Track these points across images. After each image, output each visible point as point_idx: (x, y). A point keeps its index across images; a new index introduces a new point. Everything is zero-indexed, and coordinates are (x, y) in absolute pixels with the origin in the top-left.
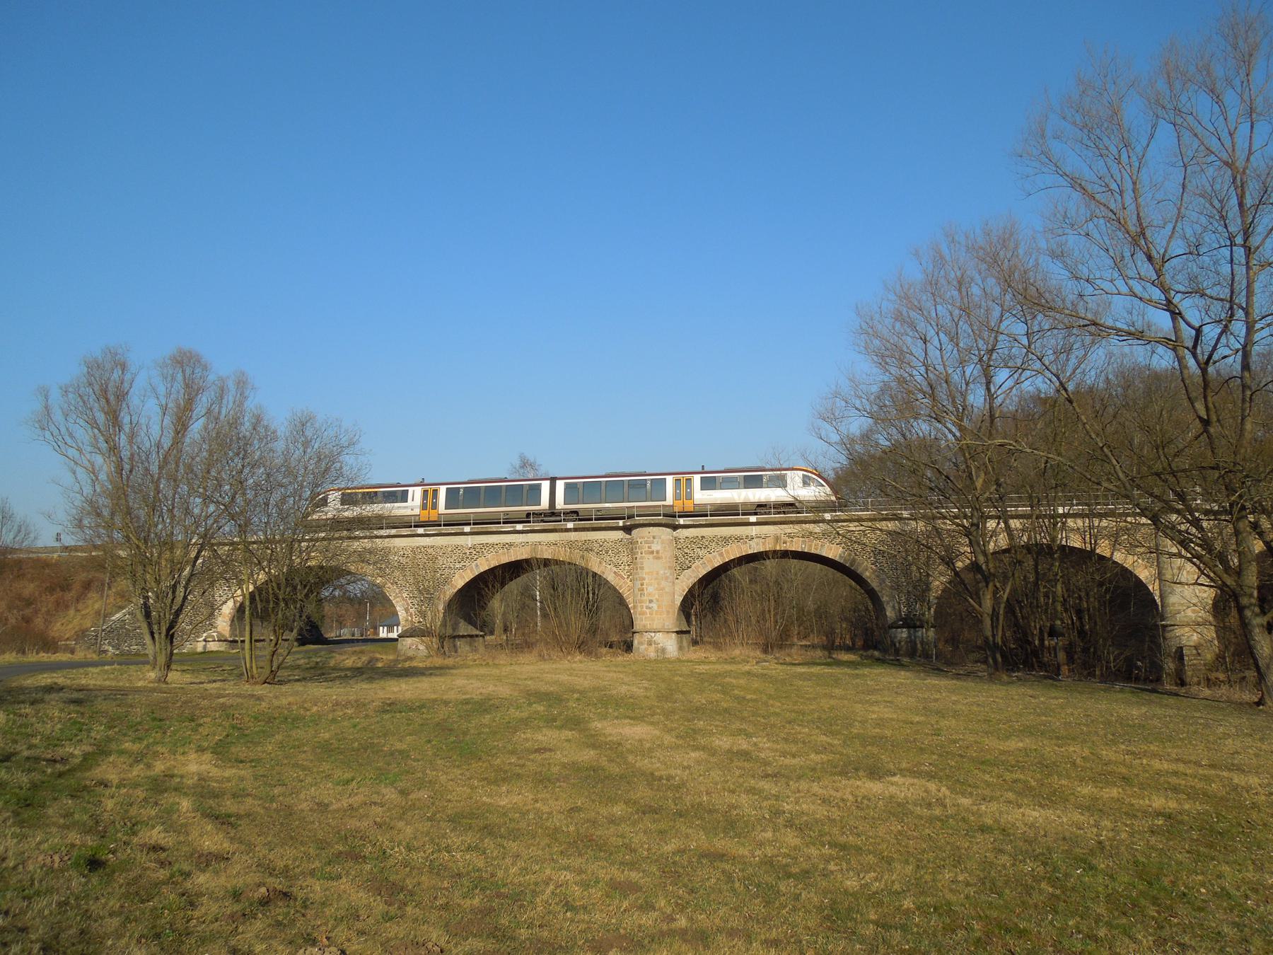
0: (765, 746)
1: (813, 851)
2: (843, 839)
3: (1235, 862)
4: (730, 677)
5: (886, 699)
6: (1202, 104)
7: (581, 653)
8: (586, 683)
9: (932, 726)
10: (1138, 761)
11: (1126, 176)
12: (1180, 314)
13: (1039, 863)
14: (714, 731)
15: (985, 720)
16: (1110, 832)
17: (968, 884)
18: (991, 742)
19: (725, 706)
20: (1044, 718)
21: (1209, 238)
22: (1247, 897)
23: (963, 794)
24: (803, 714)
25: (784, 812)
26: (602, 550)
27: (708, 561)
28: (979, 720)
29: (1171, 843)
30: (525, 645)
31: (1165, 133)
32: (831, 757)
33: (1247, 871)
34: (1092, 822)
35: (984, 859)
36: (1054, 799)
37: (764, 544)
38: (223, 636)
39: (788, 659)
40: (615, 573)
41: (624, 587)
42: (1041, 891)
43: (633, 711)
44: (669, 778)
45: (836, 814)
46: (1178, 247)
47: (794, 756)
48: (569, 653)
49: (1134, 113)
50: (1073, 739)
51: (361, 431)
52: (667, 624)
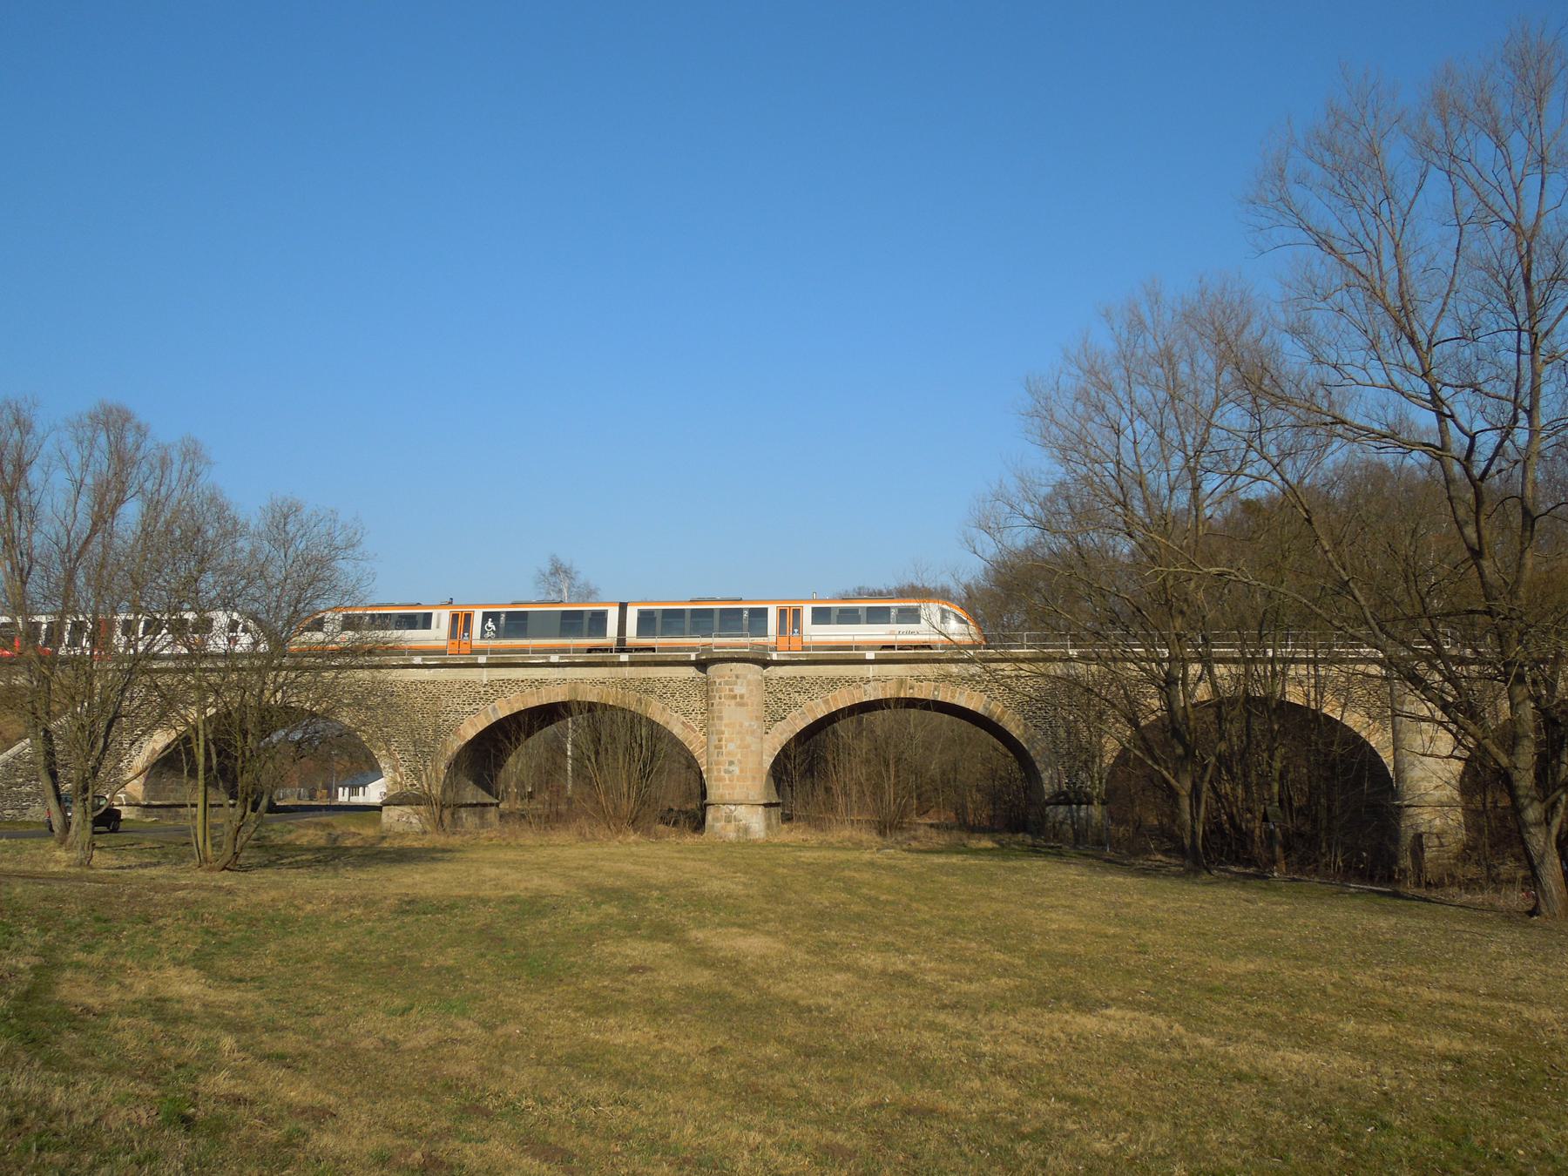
0: (931, 969)
1: (1040, 1106)
2: (1070, 1090)
3: (1549, 1117)
4: (850, 870)
5: (1064, 902)
6: (1484, 149)
8: (662, 875)
9: (1133, 941)
10: (1403, 989)
11: (1384, 234)
12: (1452, 416)
13: (1320, 1120)
15: (1199, 933)
16: (1394, 1081)
17: (1242, 1147)
18: (1213, 963)
20: (1272, 931)
21: (1486, 319)
24: (962, 922)
26: (667, 691)
27: (808, 711)
28: (1191, 934)
29: (1469, 1094)
30: (553, 819)
32: (1018, 982)
34: (1368, 1068)
35: (1252, 1116)
37: (883, 689)
38: (134, 798)
40: (683, 723)
41: (694, 742)
42: (1333, 1155)
44: (820, 1009)
46: (1447, 329)
47: (970, 980)
48: (619, 832)
49: (1398, 156)
52: (752, 793)
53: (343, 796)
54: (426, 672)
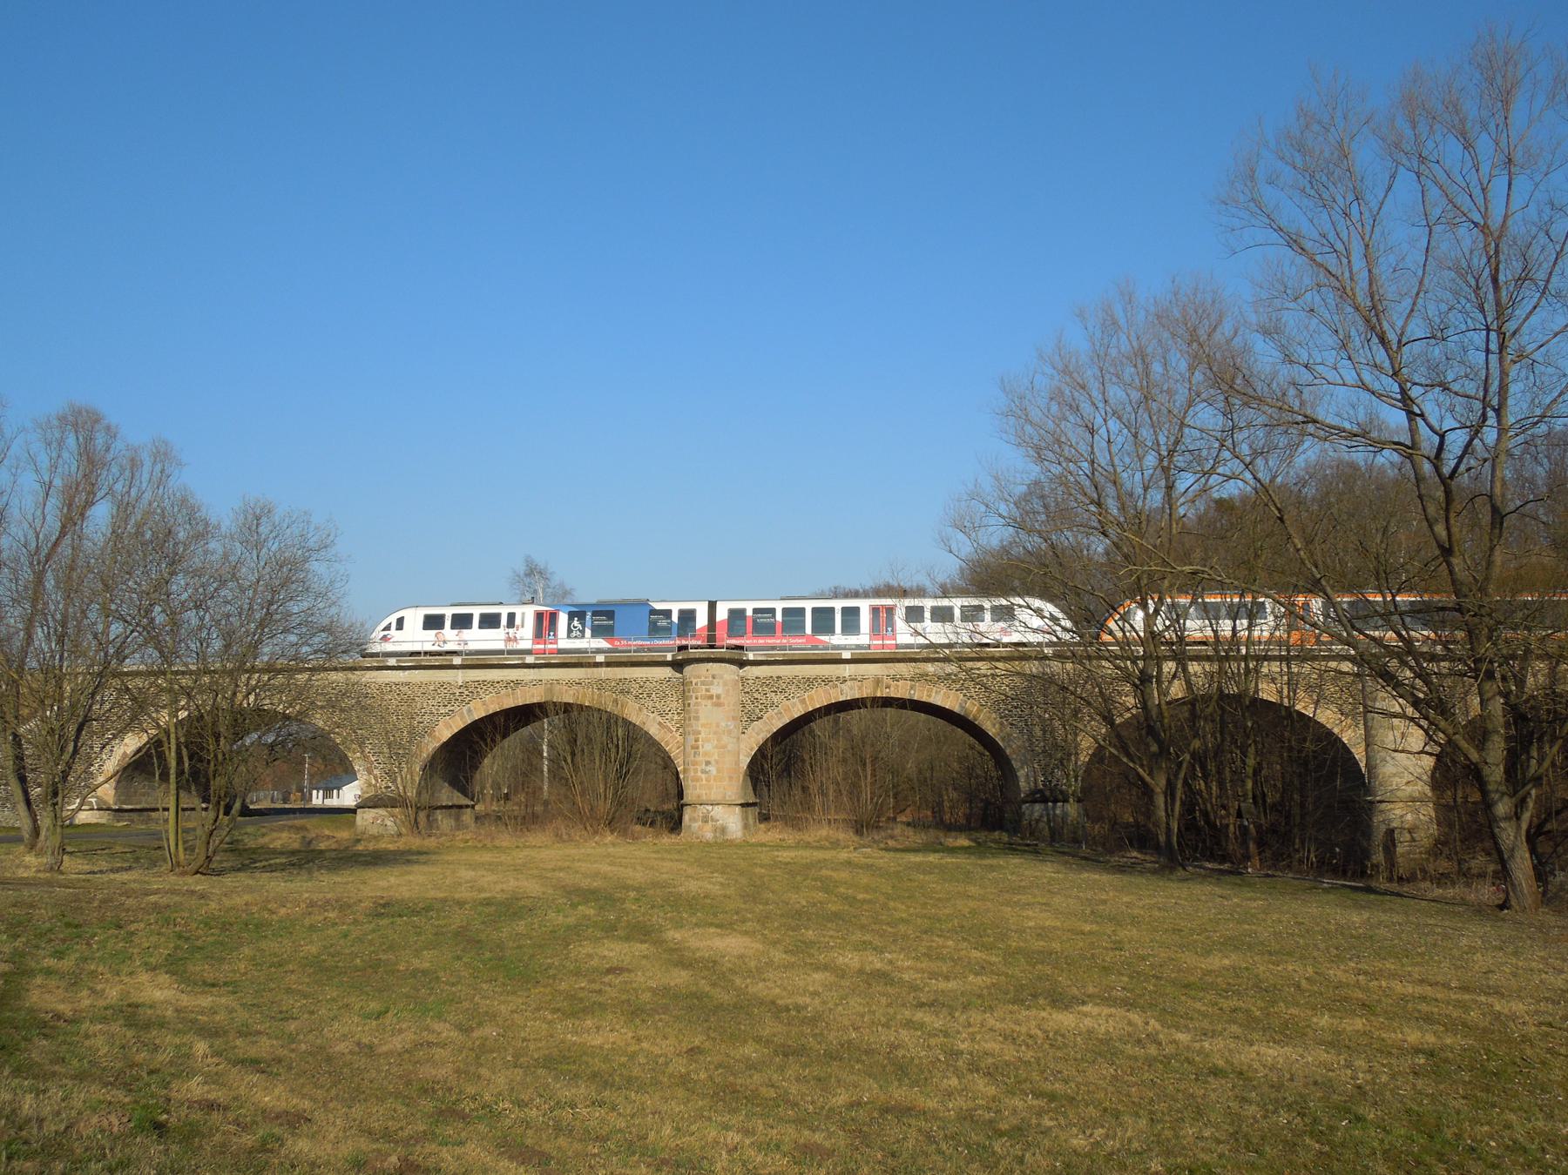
0: (907, 966)
1: (1017, 1102)
2: (1048, 1087)
4: (827, 869)
6: (1452, 151)
7: (612, 832)
9: (1109, 937)
10: (1376, 983)
12: (1422, 415)
14: (831, 944)
17: (1219, 1142)
18: (1189, 959)
19: (834, 909)
20: (1247, 927)
22: (1543, 1150)
23: (1177, 1028)
24: (939, 920)
25: (962, 1053)
26: (643, 693)
28: (1167, 930)
30: (529, 821)
31: (1406, 184)
33: (1537, 1119)
34: (1342, 1062)
36: (1288, 1032)
37: (860, 688)
38: (105, 803)
39: (891, 843)
40: (660, 723)
41: (671, 742)
42: (1307, 1148)
43: (715, 915)
44: (798, 1008)
45: (1029, 1055)
46: (1417, 329)
47: (947, 978)
48: (596, 832)
49: (1367, 156)
50: (1290, 954)
51: (337, 529)
53: (317, 799)
54: (400, 673)
